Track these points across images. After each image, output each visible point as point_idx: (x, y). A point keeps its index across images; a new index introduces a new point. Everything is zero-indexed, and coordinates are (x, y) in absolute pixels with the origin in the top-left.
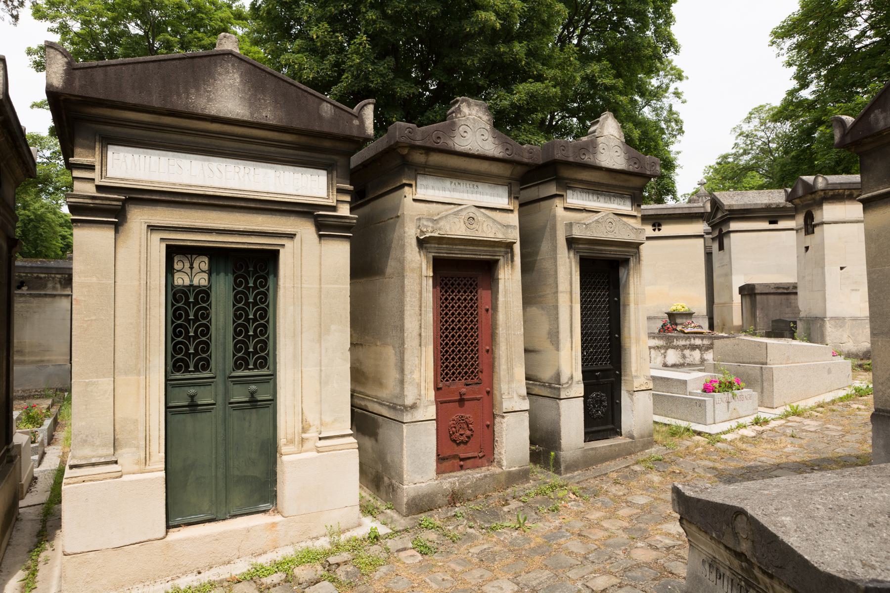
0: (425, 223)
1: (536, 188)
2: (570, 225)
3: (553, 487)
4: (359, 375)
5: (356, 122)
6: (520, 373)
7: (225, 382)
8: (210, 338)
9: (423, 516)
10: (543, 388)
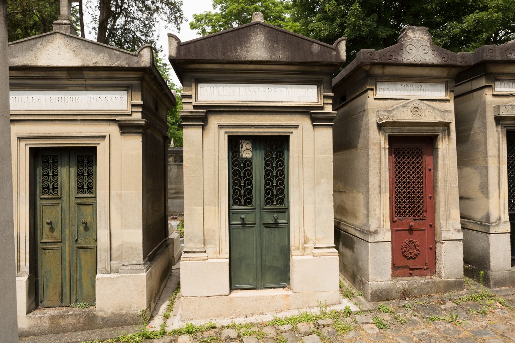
0: (382, 113)
1: (469, 83)
2: (498, 107)
3: (482, 296)
4: (341, 210)
5: (334, 53)
6: (456, 213)
7: (260, 212)
8: (252, 187)
9: (381, 303)
10: (475, 225)
